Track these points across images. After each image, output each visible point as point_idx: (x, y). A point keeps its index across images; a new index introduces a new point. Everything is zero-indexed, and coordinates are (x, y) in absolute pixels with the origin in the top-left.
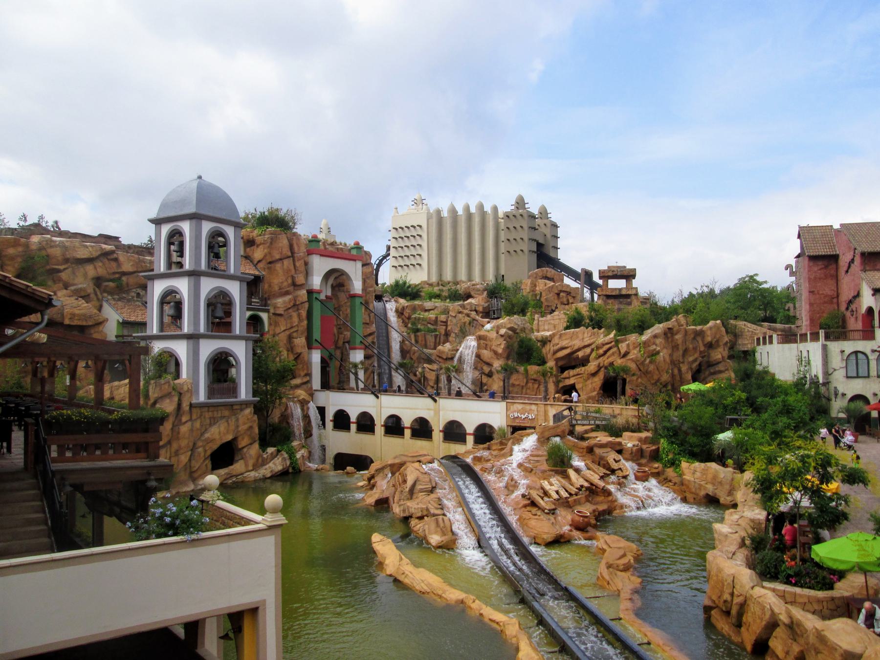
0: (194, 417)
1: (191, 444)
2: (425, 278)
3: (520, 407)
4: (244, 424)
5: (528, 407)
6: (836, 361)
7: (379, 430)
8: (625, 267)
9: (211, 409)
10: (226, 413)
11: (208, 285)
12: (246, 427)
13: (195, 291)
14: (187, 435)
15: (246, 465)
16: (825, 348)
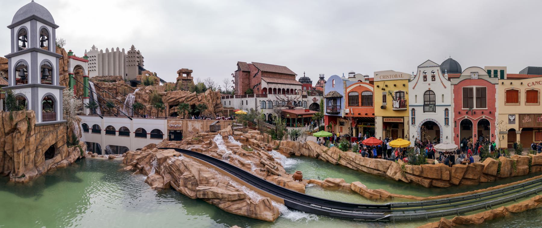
0: (36, 132)
1: (35, 147)
2: (97, 75)
3: (174, 122)
4: (61, 134)
5: (178, 122)
6: (259, 104)
7: (103, 132)
8: (187, 69)
9: (44, 127)
10: (52, 129)
11: (41, 58)
12: (61, 136)
13: (34, 61)
14: (33, 143)
15: (62, 157)
16: (256, 99)
